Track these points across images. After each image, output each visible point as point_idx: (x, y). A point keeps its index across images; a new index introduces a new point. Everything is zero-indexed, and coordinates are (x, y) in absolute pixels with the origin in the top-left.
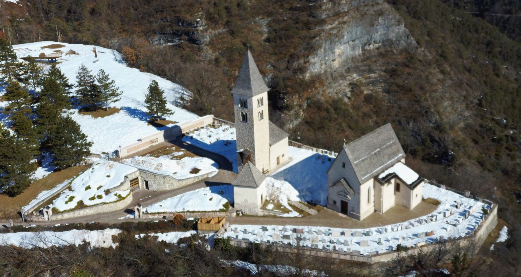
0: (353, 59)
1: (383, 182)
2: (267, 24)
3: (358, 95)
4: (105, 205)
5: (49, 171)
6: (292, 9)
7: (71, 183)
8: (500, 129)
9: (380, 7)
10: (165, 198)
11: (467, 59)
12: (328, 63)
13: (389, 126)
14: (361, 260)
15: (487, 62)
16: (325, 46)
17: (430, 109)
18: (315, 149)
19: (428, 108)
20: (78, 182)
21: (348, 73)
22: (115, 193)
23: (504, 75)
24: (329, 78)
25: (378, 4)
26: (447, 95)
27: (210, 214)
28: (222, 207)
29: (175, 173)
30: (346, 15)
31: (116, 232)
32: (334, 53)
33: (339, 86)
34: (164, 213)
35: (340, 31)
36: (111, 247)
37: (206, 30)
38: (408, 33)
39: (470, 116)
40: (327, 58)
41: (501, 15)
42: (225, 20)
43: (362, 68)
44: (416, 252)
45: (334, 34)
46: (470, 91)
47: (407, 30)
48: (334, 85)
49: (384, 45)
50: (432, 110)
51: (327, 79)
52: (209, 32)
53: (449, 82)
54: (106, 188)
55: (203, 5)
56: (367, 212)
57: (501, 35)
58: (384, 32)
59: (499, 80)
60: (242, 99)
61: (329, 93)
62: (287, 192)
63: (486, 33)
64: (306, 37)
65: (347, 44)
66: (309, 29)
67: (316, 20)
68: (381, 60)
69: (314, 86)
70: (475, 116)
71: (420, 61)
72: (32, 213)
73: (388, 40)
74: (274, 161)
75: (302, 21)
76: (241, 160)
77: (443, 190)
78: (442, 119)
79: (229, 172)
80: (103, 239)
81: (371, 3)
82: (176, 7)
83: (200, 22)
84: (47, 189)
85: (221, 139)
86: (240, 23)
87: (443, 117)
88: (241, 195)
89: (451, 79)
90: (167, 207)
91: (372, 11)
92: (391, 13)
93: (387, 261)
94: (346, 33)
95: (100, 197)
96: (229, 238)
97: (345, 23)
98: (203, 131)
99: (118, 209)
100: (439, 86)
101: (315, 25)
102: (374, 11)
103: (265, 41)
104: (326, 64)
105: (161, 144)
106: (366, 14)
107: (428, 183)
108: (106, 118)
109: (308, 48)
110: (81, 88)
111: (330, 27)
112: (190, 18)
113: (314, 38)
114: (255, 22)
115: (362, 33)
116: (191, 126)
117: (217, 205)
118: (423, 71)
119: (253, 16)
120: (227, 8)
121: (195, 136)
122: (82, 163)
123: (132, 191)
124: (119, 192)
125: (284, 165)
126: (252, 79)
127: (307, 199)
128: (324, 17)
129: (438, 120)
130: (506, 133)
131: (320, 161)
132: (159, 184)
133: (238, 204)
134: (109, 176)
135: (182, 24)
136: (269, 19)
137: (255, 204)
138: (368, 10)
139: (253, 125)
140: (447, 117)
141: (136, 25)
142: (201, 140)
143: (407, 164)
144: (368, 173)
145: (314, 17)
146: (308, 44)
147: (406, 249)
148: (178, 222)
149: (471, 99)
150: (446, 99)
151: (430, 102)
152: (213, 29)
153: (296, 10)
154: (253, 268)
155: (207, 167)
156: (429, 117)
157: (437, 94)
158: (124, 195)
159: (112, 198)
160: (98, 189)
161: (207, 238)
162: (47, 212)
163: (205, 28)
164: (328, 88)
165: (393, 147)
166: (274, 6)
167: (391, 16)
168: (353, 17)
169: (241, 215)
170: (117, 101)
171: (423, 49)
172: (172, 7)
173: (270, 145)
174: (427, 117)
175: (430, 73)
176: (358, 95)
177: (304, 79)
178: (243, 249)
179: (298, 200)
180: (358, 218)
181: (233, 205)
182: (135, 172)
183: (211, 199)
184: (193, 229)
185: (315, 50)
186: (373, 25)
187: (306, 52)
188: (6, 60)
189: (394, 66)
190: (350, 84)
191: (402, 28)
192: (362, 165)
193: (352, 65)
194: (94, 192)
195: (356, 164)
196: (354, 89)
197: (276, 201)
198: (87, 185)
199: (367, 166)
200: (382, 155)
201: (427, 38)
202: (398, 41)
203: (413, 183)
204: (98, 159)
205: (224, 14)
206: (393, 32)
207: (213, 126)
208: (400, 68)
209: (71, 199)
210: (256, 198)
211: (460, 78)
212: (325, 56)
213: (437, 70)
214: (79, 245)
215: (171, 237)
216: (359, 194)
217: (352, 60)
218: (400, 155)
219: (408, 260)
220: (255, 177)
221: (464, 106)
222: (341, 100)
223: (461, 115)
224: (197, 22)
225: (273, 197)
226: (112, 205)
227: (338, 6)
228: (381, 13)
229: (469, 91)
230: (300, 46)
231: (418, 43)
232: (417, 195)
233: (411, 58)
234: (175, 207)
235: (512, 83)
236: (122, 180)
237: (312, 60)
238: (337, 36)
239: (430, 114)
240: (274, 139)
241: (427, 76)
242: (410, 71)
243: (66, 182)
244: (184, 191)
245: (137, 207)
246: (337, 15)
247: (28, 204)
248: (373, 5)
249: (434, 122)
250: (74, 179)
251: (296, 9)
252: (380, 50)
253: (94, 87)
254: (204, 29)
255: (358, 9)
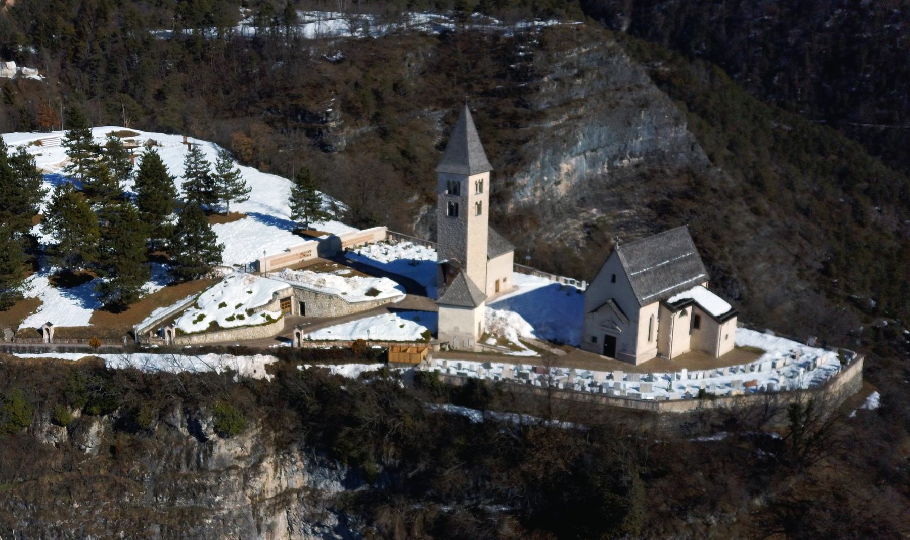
0: (592, 182)
1: (675, 308)
2: (443, 119)
3: (599, 246)
4: (248, 329)
5: (160, 284)
6: (487, 93)
7: (196, 299)
8: (864, 315)
9: (644, 92)
10: (334, 325)
11: (803, 192)
12: (547, 187)
13: (684, 230)
14: (642, 407)
15: (842, 200)
16: (544, 157)
17: (730, 273)
18: (554, 277)
19: (726, 272)
20: (207, 298)
21: (582, 207)
22: (263, 312)
23: (874, 224)
24: (548, 214)
25: (640, 87)
26: (763, 252)
27: (402, 345)
28: (420, 337)
29: (344, 294)
30: (582, 105)
31: (269, 359)
32: (558, 170)
33: (565, 228)
34: (335, 341)
35: (570, 131)
36: (264, 379)
37: (341, 128)
38: (693, 140)
39: (806, 290)
40: (546, 179)
41: (870, 126)
42: (373, 111)
43: (607, 199)
44: (728, 403)
45: (561, 137)
46: (807, 247)
47: (692, 135)
48: (556, 227)
49: (648, 161)
50: (735, 276)
51: (544, 214)
52: (345, 130)
53: (767, 230)
54: (249, 307)
55: (338, 86)
56: (646, 353)
57: (870, 158)
58: (650, 137)
59: (864, 232)
60: (451, 180)
61: (548, 239)
62: (517, 325)
63: (840, 154)
64: (511, 140)
65: (583, 156)
66: (517, 127)
67: (529, 112)
68: (643, 185)
69: (522, 225)
70: (816, 291)
71: (714, 190)
72: (148, 334)
73: (655, 151)
74: (491, 286)
75: (504, 114)
76: (443, 278)
77: (770, 337)
78: (752, 293)
79: (422, 298)
80: (256, 367)
81: (627, 86)
82: (292, 88)
83: (333, 114)
84: (164, 306)
85: (403, 258)
86: (396, 117)
87: (755, 289)
88: (450, 320)
89: (771, 224)
90: (340, 334)
91: (628, 99)
92: (663, 103)
93: (682, 411)
94: (581, 136)
95: (241, 317)
96: (437, 372)
97: (580, 118)
98: (373, 247)
99: (267, 336)
100: (748, 235)
101: (528, 120)
102: (633, 100)
103: (437, 147)
104: (543, 189)
105: (316, 259)
106: (617, 103)
107: (744, 327)
108: (227, 224)
109: (513, 160)
110: (190, 180)
111: (553, 124)
112: (316, 108)
113: (524, 142)
114: (422, 116)
115: (609, 136)
116: (356, 239)
117: (413, 334)
118: (718, 208)
119: (418, 106)
120: (376, 92)
121: (363, 252)
122: (209, 276)
123: (284, 314)
124: (267, 313)
125: (505, 293)
126: (469, 149)
127: (548, 337)
128: (543, 106)
129: (746, 293)
130: (874, 323)
131: (564, 293)
132: (321, 307)
133: (444, 333)
134: (250, 292)
135: (303, 118)
136: (446, 111)
137: (470, 334)
138: (621, 98)
139: (466, 222)
140: (762, 290)
141: (227, 118)
142: (374, 259)
143: (709, 288)
144: (651, 293)
145: (526, 106)
146: (514, 152)
147: (712, 397)
148: (358, 351)
149: (809, 260)
150: (760, 259)
151: (730, 262)
152: (352, 126)
153: (493, 96)
154: (475, 416)
155: (388, 289)
156: (729, 287)
157: (745, 248)
158: (275, 316)
159: (258, 319)
160: (237, 307)
161: (402, 372)
162: (169, 332)
163: (339, 124)
164: (546, 230)
165: (690, 263)
166: (455, 89)
167: (663, 110)
168: (594, 109)
169: (448, 349)
170: (243, 200)
171: (720, 170)
172: (286, 89)
173: (488, 258)
174: (725, 287)
175: (733, 213)
176: (599, 246)
177: (504, 213)
178: (457, 389)
179: (533, 337)
180: (633, 360)
181: (435, 335)
182: (287, 289)
183: (402, 326)
184: (380, 362)
185: (525, 164)
186: (630, 124)
187: (510, 166)
188: (78, 139)
189: (665, 198)
190: (586, 226)
191: (683, 131)
192: (643, 279)
193: (588, 193)
194: (230, 311)
195: (634, 277)
196: (593, 234)
197: (499, 336)
198: (221, 302)
199: (651, 283)
200: (672, 271)
201: (726, 152)
202: (674, 153)
203: (722, 315)
204: (230, 271)
205: (371, 101)
206: (665, 137)
207: (387, 242)
208: (678, 201)
209: (201, 318)
210: (473, 324)
211: (789, 223)
212: (542, 175)
213: (745, 207)
214: (221, 373)
215: (348, 370)
216: (636, 322)
217: (590, 185)
218: (701, 275)
219: (715, 415)
220: (472, 294)
221: (794, 272)
222: (568, 251)
223: (789, 288)
224: (328, 114)
225: (495, 330)
226: (258, 328)
227: (569, 90)
228: (644, 104)
229: (806, 247)
230: (499, 155)
231: (711, 157)
232: (727, 336)
233: (699, 183)
234: (351, 334)
235: (890, 238)
236: (271, 298)
237: (520, 181)
238: (564, 141)
239: (729, 281)
240: (494, 250)
241: (726, 217)
242: (694, 206)
243: (189, 299)
244: (362, 317)
245: (297, 330)
246: (567, 104)
247: (141, 322)
248: (630, 90)
249: (737, 297)
250: (200, 295)
251: (494, 93)
252: (641, 167)
253: (209, 181)
254: (338, 126)
255: (603, 95)
